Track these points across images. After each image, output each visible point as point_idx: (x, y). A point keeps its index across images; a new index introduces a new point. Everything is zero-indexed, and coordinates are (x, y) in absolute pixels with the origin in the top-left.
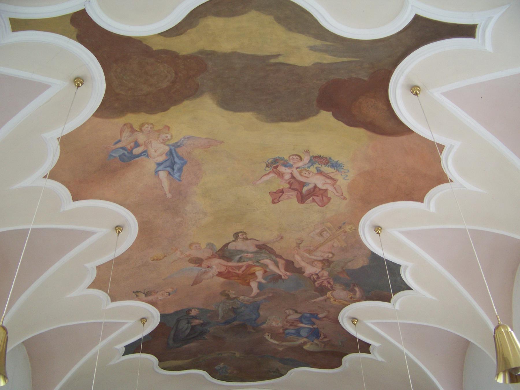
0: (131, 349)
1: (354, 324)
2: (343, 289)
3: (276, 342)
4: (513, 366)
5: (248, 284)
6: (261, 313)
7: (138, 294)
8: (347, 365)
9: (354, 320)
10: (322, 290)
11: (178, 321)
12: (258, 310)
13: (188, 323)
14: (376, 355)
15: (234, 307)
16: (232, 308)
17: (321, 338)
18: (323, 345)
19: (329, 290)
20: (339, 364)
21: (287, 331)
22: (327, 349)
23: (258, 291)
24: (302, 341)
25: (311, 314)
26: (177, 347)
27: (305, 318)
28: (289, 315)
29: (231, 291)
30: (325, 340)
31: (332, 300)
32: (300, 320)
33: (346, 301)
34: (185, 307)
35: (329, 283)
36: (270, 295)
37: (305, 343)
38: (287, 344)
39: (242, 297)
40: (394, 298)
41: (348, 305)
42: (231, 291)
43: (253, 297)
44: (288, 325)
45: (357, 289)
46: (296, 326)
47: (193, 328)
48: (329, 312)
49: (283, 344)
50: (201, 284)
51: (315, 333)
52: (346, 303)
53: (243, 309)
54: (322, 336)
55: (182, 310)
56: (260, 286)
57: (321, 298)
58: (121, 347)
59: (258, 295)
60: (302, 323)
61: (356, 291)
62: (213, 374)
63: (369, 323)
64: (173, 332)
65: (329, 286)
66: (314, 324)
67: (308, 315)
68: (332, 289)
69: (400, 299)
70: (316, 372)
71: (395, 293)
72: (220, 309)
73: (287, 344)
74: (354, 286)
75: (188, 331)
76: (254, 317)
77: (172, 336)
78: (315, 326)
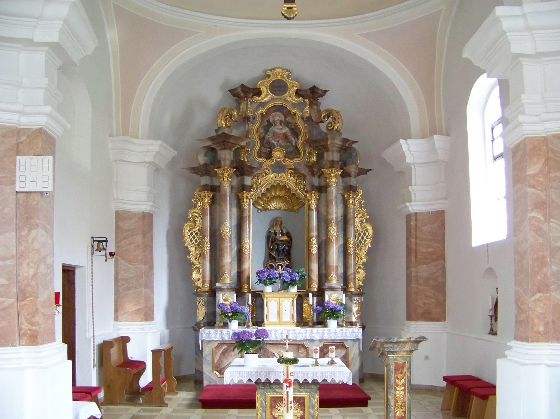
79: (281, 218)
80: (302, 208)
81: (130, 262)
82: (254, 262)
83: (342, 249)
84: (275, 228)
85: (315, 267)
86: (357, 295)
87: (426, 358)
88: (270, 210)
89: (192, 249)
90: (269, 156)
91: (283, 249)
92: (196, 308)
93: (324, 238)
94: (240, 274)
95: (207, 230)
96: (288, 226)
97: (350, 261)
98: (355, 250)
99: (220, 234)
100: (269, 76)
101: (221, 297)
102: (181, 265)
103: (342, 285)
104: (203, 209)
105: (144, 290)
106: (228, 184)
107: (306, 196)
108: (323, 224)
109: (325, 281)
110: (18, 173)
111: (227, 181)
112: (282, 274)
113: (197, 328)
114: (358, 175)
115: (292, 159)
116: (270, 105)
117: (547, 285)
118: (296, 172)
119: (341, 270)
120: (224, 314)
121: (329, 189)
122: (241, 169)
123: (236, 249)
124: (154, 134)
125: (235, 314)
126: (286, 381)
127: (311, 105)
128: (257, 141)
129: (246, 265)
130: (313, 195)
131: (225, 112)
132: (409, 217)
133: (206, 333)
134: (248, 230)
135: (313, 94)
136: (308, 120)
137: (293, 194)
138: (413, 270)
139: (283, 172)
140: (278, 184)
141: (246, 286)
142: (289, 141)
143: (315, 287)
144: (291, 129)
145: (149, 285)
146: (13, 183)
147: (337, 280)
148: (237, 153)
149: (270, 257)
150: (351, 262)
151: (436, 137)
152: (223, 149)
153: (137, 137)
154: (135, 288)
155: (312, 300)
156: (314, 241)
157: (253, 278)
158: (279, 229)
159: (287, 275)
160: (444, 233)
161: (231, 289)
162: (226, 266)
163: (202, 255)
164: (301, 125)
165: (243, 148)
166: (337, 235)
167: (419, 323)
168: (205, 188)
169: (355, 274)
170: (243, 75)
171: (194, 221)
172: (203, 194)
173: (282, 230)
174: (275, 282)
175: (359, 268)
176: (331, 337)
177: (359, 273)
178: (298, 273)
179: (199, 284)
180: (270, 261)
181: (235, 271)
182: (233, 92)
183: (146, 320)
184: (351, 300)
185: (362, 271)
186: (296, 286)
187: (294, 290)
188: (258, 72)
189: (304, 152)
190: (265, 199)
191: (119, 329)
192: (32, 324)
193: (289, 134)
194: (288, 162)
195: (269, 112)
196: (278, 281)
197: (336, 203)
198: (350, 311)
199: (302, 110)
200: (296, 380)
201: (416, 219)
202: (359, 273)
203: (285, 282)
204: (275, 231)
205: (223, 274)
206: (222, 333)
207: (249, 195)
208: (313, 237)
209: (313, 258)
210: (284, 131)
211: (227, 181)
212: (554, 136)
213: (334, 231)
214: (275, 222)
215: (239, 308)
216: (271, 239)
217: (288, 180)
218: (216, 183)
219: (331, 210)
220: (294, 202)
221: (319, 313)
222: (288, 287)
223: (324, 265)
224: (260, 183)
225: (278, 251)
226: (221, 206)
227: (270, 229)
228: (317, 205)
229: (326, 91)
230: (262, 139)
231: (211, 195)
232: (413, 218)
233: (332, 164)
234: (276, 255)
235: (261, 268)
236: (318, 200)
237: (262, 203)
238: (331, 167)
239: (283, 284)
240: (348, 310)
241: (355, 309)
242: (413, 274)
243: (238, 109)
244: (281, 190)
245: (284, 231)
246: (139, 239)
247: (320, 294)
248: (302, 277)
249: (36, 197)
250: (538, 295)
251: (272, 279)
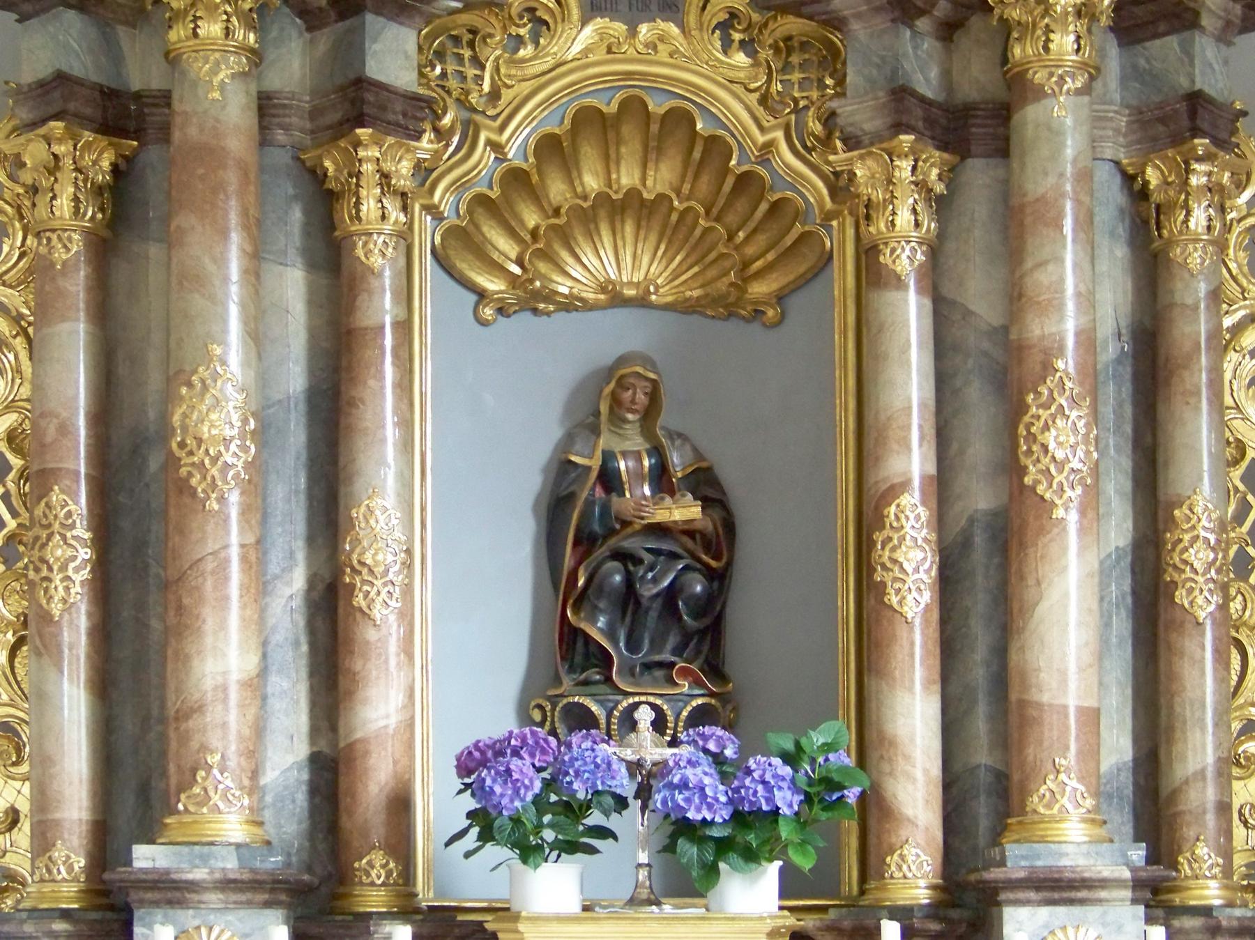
79: (648, 362)
80: (817, 285)
82: (449, 665)
83: (1121, 586)
84: (605, 441)
85: (914, 716)
88: (570, 305)
91: (671, 594)
93: (980, 497)
94: (330, 772)
95: (65, 429)
96: (707, 423)
97: (1187, 672)
99: (172, 462)
103: (1138, 854)
106: (238, 63)
107: (840, 185)
108: (977, 397)
109: (998, 833)
112: (662, 768)
119: (1118, 747)
121: (1031, 114)
123: (298, 580)
129: (379, 709)
130: (904, 168)
134: (391, 433)
137: (745, 180)
140: (633, 107)
141: (375, 867)
147: (1095, 820)
149: (569, 653)
157: (440, 805)
158: (637, 442)
159: (703, 775)
161: (255, 888)
162: (213, 714)
166: (1096, 470)
168: (53, 98)
172: (35, 152)
173: (657, 451)
174: (604, 833)
176: (71, 68)
178: (790, 759)
180: (567, 682)
181: (288, 755)
186: (772, 870)
190: (531, 218)
197: (1086, 223)
203: (684, 828)
204: (608, 457)
207: (406, 167)
208: (905, 486)
209: (898, 655)
213: (1071, 442)
214: (615, 394)
216: (577, 526)
218: (141, 74)
219: (1043, 277)
220: (754, 246)
222: (711, 872)
223: (982, 710)
224: (495, 95)
227: (568, 441)
228: (935, 250)
231: (102, 160)
234: (611, 634)
235: (497, 719)
236: (942, 206)
237: (504, 245)
239: (670, 848)
244: (650, 153)
245: (678, 461)
248: (822, 792)
251: (587, 806)
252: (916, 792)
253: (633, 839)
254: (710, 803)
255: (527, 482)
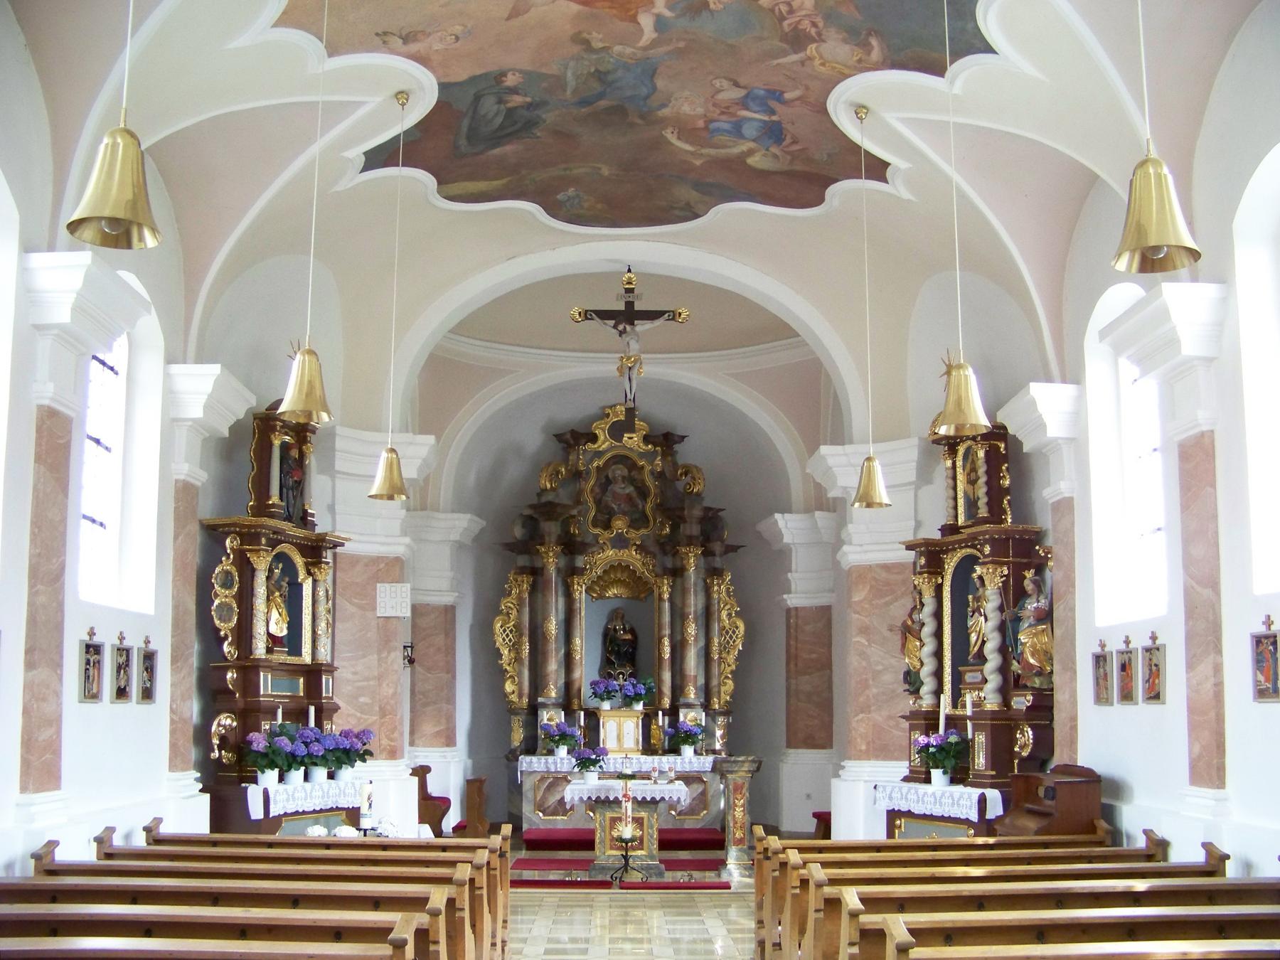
0: (376, 159)
1: (861, 119)
2: (845, 41)
3: (688, 147)
4: (1152, 242)
5: (634, 19)
6: (660, 83)
7: (386, 39)
8: (836, 202)
9: (860, 111)
10: (798, 40)
11: (478, 98)
12: (652, 76)
13: (500, 101)
14: (896, 187)
15: (601, 69)
16: (597, 70)
17: (784, 143)
18: (789, 157)
19: (814, 41)
20: (819, 200)
21: (712, 126)
22: (798, 167)
23: (655, 35)
24: (744, 147)
25: (768, 91)
26: (477, 154)
27: (755, 98)
28: (719, 91)
29: (595, 34)
30: (795, 148)
31: (817, 62)
32: (743, 103)
33: (849, 67)
34: (492, 67)
35: (814, 25)
36: (681, 45)
37: (751, 152)
38: (712, 152)
39: (617, 48)
40: (952, 70)
41: (850, 76)
42: (595, 34)
43: (645, 49)
44: (718, 112)
45: (874, 42)
46: (734, 115)
47: (510, 112)
48: (807, 88)
49: (704, 151)
50: (526, 16)
51: (774, 133)
52: (846, 71)
53: (620, 73)
54: (788, 140)
55: (486, 74)
56: (660, 23)
57: (795, 57)
58: (356, 154)
59: (654, 44)
60: (747, 109)
61: (873, 48)
62: (553, 210)
63: (893, 119)
64: (466, 123)
65: (813, 31)
66: (773, 112)
67: (762, 92)
68: (820, 39)
69: (966, 70)
70: (771, 214)
71: (957, 55)
72: (569, 74)
73: (712, 152)
74: (869, 34)
75: (499, 120)
76: (644, 91)
77: (465, 129)
78: (774, 118)
81: (429, 670)
82: (587, 670)
85: (667, 676)
86: (722, 714)
87: (808, 796)
89: (505, 652)
90: (607, 526)
92: (510, 730)
93: (679, 638)
94: (568, 685)
98: (720, 654)
100: (608, 415)
101: (545, 716)
102: (489, 671)
104: (520, 598)
105: (445, 706)
110: (379, 600)
111: (552, 562)
113: (512, 757)
114: (726, 552)
115: (638, 529)
116: (609, 455)
117: (869, 707)
118: (641, 549)
119: (701, 681)
120: (550, 736)
122: (571, 547)
124: (459, 506)
125: (564, 737)
126: (625, 796)
127: (664, 455)
128: (591, 504)
129: (577, 674)
131: (550, 469)
132: (788, 610)
133: (528, 763)
135: (666, 440)
136: (660, 476)
137: (640, 578)
138: (793, 681)
139: (626, 547)
140: (620, 564)
141: (576, 701)
142: (634, 505)
143: (666, 702)
144: (637, 488)
145: (451, 700)
146: (374, 609)
148: (565, 525)
150: (715, 671)
151: (817, 513)
152: (547, 520)
153: (438, 510)
154: (435, 703)
155: (662, 720)
156: (666, 642)
157: (586, 691)
159: (631, 688)
160: (830, 636)
161: (557, 705)
163: (518, 659)
164: (650, 483)
165: (573, 517)
167: (800, 751)
168: (522, 571)
169: (719, 685)
170: (570, 413)
171: (508, 614)
175: (727, 677)
177: (725, 684)
179: (514, 698)
181: (562, 681)
182: (559, 437)
183: (448, 745)
184: (714, 721)
185: (730, 682)
187: (639, 707)
188: (592, 410)
189: (655, 520)
191: (416, 757)
192: (391, 740)
193: (634, 495)
194: (633, 534)
195: (607, 464)
196: (619, 694)
197: (695, 591)
198: (713, 735)
199: (652, 463)
200: (635, 798)
201: (797, 617)
202: (725, 684)
205: (546, 686)
206: (547, 762)
210: (627, 491)
211: (552, 562)
212: (878, 565)
214: (615, 615)
215: (569, 730)
216: (609, 639)
217: (632, 557)
218: (538, 564)
220: (640, 589)
221: (672, 737)
225: (618, 654)
226: (544, 596)
228: (671, 594)
229: (684, 437)
230: (598, 502)
232: (793, 613)
233: (690, 541)
235: (597, 678)
238: (689, 545)
240: (709, 733)
241: (719, 733)
242: (793, 687)
243: (566, 461)
246: (440, 640)
247: (673, 712)
248: (649, 690)
249: (394, 622)
250: (861, 716)
252: (667, 689)
253: (618, 699)
254: (631, 693)
255: (601, 630)
